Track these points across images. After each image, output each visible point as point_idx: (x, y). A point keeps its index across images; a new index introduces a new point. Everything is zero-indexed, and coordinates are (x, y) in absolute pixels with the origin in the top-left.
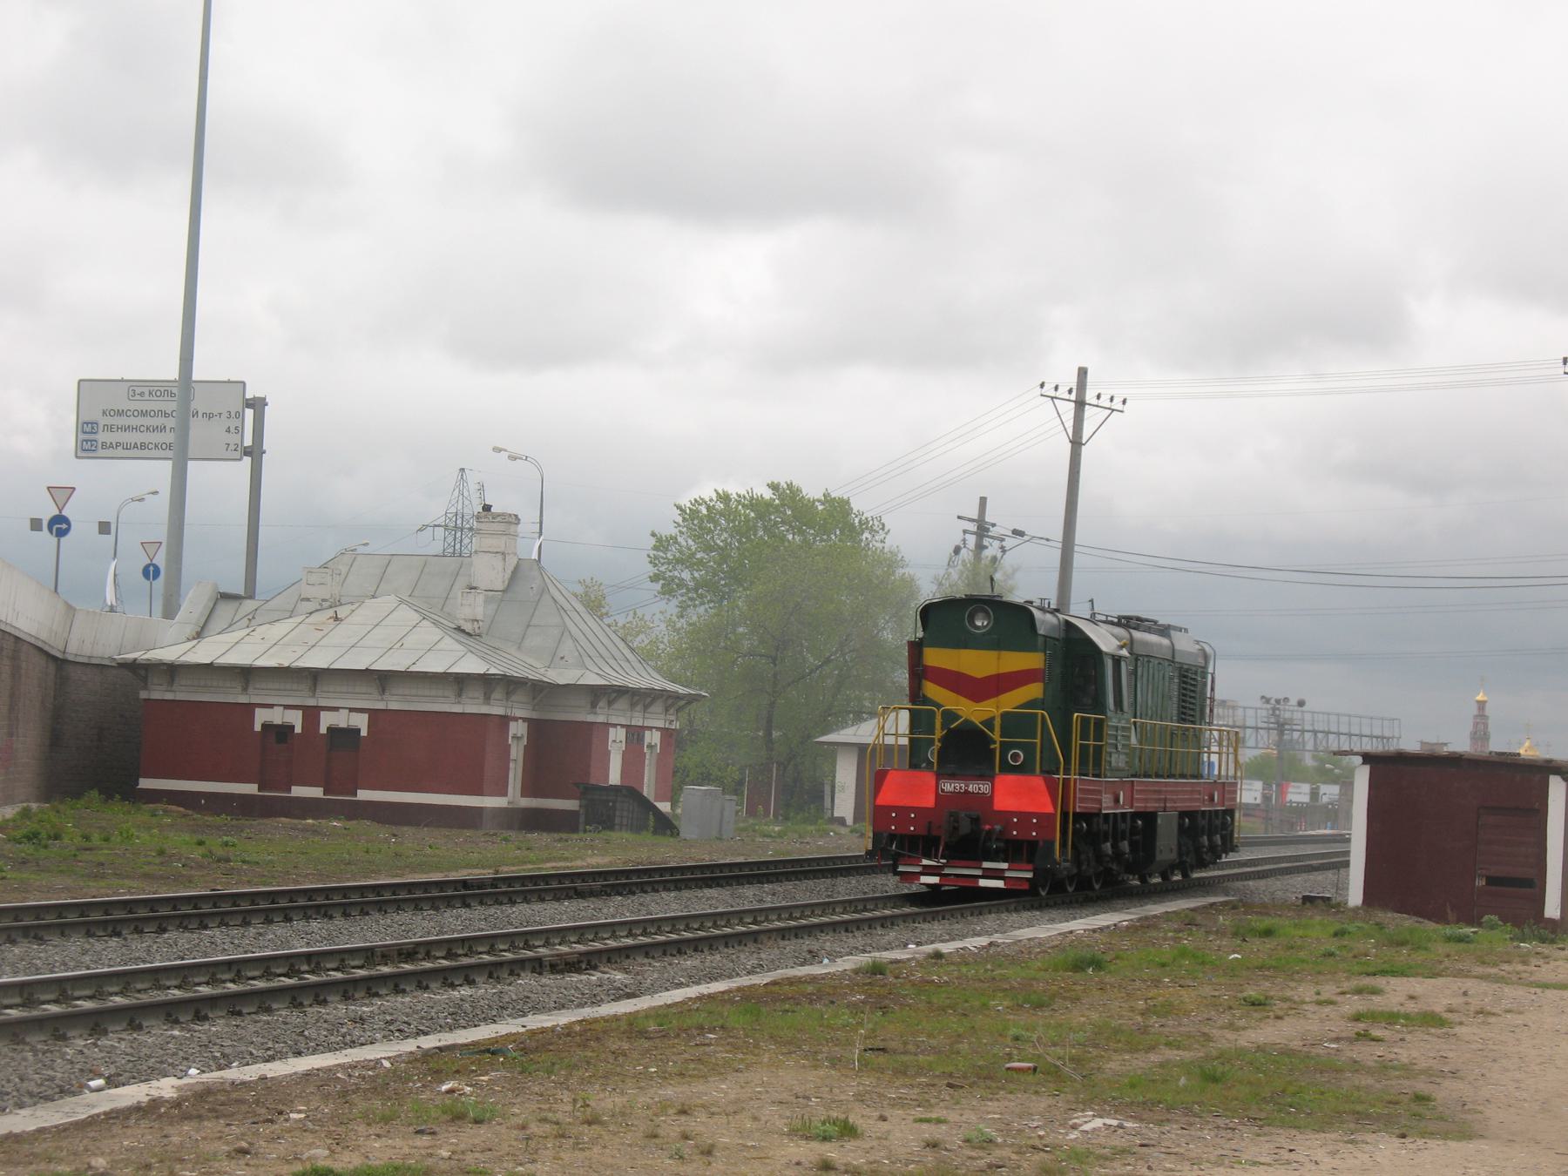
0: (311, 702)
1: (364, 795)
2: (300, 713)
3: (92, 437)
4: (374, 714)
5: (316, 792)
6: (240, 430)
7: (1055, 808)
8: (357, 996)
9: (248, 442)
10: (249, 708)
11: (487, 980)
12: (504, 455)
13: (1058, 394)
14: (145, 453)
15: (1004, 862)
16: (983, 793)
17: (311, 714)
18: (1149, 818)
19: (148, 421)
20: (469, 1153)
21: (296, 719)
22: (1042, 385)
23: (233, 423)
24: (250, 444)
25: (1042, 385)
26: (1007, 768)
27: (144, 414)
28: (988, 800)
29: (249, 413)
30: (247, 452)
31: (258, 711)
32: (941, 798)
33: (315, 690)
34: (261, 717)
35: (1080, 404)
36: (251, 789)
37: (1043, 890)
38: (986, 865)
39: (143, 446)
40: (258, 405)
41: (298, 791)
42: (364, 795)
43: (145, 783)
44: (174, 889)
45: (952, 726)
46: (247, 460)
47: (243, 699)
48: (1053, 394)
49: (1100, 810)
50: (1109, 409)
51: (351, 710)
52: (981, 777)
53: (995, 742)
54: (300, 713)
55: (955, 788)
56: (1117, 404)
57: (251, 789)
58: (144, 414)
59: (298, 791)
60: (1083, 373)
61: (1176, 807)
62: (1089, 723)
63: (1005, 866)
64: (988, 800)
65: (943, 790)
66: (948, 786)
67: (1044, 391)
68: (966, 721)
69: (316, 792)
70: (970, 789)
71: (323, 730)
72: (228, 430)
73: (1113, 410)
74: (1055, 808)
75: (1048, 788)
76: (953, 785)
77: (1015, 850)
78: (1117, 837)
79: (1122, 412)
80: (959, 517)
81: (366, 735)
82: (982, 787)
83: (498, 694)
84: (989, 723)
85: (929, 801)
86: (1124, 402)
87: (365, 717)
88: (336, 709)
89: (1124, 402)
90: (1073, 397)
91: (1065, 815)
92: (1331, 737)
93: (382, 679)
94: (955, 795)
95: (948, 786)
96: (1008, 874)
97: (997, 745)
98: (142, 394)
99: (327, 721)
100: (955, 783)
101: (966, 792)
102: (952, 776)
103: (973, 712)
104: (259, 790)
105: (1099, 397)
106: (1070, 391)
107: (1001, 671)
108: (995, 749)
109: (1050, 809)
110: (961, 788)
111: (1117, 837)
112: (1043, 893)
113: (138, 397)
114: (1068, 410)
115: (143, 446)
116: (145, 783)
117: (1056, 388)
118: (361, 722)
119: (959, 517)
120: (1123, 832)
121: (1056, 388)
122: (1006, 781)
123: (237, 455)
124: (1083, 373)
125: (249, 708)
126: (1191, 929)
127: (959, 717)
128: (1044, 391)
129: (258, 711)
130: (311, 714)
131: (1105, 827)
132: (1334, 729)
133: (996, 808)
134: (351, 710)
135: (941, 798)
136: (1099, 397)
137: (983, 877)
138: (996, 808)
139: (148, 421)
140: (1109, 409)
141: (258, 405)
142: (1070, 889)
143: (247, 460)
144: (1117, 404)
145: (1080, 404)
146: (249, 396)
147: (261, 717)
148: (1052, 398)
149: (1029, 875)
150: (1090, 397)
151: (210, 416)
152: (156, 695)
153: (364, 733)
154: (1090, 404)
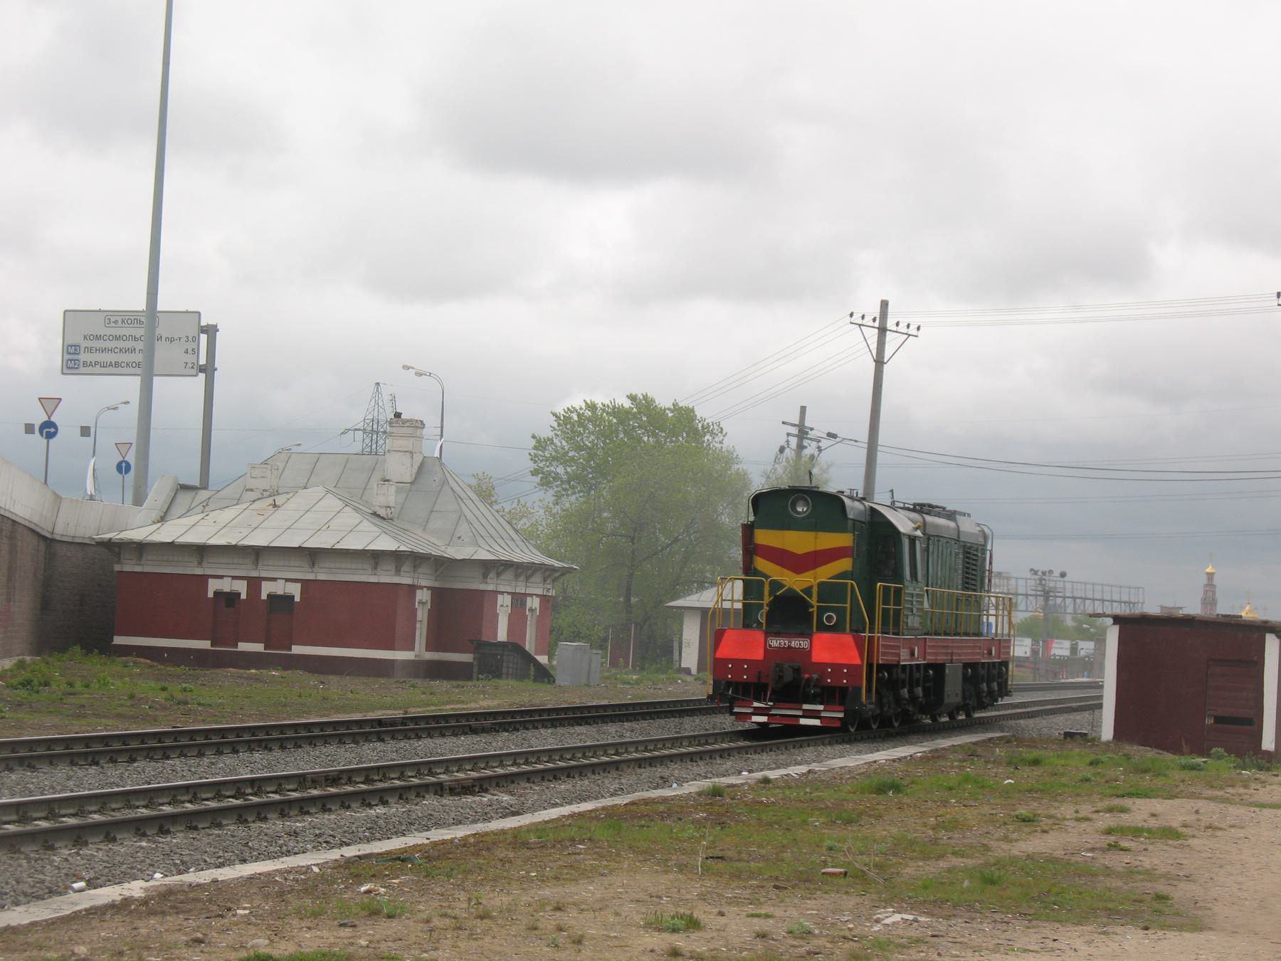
0: (254, 574)
1: (297, 650)
2: (245, 583)
3: (75, 357)
5: (258, 647)
6: (196, 352)
7: (862, 660)
9: (203, 361)
10: (204, 579)
13: (864, 322)
14: (119, 370)
16: (803, 648)
17: (254, 584)
19: (121, 344)
21: (241, 588)
22: (851, 315)
23: (191, 346)
24: (205, 363)
25: (851, 315)
27: (117, 338)
28: (807, 654)
29: (204, 337)
30: (202, 369)
31: (211, 581)
32: (768, 652)
33: (257, 564)
34: (213, 586)
35: (883, 330)
36: (205, 644)
39: (117, 365)
40: (211, 331)
41: (244, 647)
42: (297, 650)
43: (119, 640)
45: (778, 594)
46: (202, 376)
47: (198, 571)
48: (860, 322)
49: (899, 662)
50: (906, 334)
51: (287, 580)
52: (802, 635)
54: (245, 583)
55: (780, 644)
56: (912, 330)
57: (205, 644)
58: (117, 338)
59: (244, 647)
60: (884, 304)
61: (960, 660)
62: (890, 591)
64: (807, 654)
65: (770, 646)
66: (775, 643)
67: (853, 320)
68: (790, 589)
69: (258, 647)
70: (793, 645)
71: (264, 597)
72: (186, 352)
73: (909, 335)
74: (862, 660)
75: (856, 644)
76: (778, 642)
78: (912, 684)
79: (916, 336)
80: (783, 423)
82: (802, 643)
85: (759, 655)
86: (918, 328)
87: (299, 586)
88: (274, 579)
89: (918, 328)
90: (877, 324)
91: (870, 666)
93: (312, 555)
94: (780, 650)
95: (775, 643)
98: (116, 322)
99: (267, 589)
100: (780, 640)
101: (790, 647)
102: (778, 634)
103: (795, 581)
105: (897, 324)
106: (874, 320)
109: (858, 661)
110: (785, 644)
111: (912, 684)
113: (112, 325)
114: (873, 335)
115: (117, 365)
116: (119, 640)
117: (863, 317)
118: (295, 590)
119: (783, 423)
121: (863, 317)
122: (822, 638)
123: (194, 371)
124: (884, 304)
125: (204, 579)
127: (783, 586)
128: (853, 320)
129: (211, 581)
130: (254, 584)
131: (903, 676)
133: (813, 660)
134: (287, 580)
135: (768, 652)
136: (897, 324)
138: (813, 660)
139: (121, 344)
140: (906, 334)
141: (211, 331)
142: (874, 727)
143: (202, 376)
144: (912, 330)
145: (883, 330)
147: (213, 586)
148: (860, 325)
150: (890, 324)
151: (172, 340)
152: (127, 568)
153: (297, 599)
154: (890, 331)
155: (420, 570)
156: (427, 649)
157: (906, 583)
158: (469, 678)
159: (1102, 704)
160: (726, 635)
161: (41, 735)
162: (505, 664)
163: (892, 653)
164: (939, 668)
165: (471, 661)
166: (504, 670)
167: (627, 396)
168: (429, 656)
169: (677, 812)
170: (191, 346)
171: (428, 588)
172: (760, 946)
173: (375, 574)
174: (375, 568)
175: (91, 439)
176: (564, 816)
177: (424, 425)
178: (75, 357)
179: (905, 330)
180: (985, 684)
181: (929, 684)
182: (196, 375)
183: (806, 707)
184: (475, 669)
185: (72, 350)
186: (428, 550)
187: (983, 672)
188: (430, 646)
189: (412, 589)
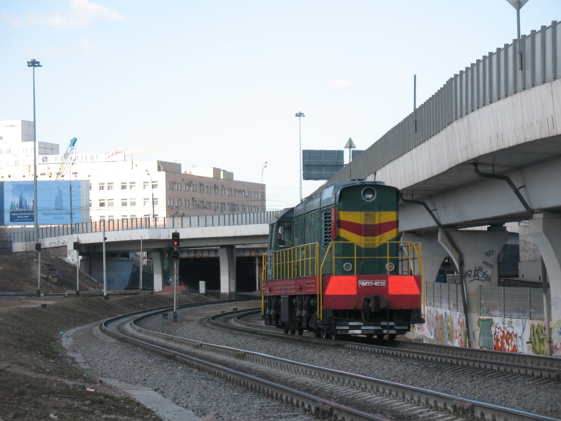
8: (244, 368)
11: (463, 405)
12: (147, 173)
16: (382, 286)
18: (279, 297)
20: (69, 336)
52: (380, 279)
55: (367, 284)
61: (287, 293)
65: (361, 285)
66: (364, 283)
76: (366, 282)
80: (415, 76)
81: (200, 282)
95: (364, 283)
100: (367, 281)
101: (374, 286)
110: (370, 284)
119: (415, 76)
126: (495, 349)
127: (385, 244)
135: (360, 289)
159: (161, 171)
163: (292, 284)
167: (350, 138)
169: (210, 407)
172: (399, 345)
175: (425, 281)
176: (112, 418)
183: (351, 324)
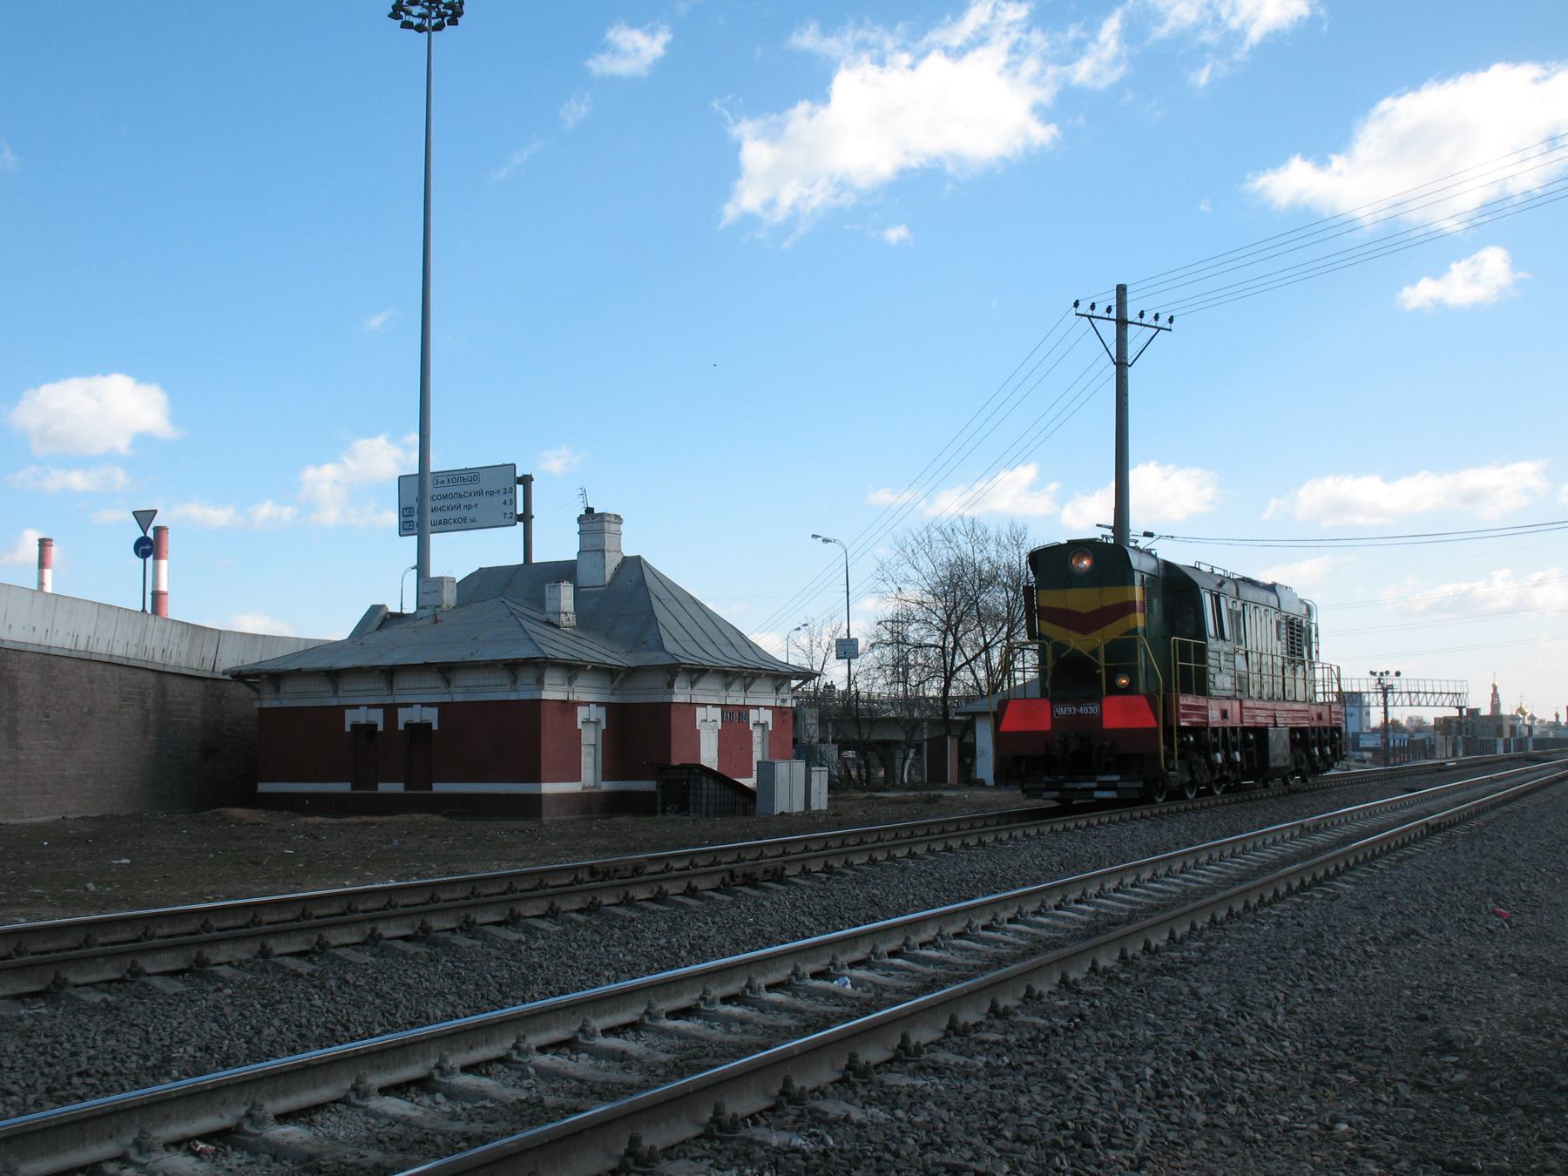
0: (389, 700)
1: (439, 788)
2: (381, 711)
3: (409, 519)
4: (442, 706)
5: (397, 788)
6: (513, 502)
7: (1157, 722)
9: (520, 511)
10: (340, 710)
13: (1095, 313)
14: (448, 527)
15: (1116, 774)
17: (391, 711)
19: (448, 502)
21: (377, 717)
22: (1076, 304)
23: (508, 497)
24: (522, 512)
25: (1076, 304)
26: (1114, 690)
27: (445, 497)
28: (1098, 719)
29: (520, 488)
30: (520, 518)
31: (400, 711)
32: (1055, 721)
33: (392, 686)
34: (351, 717)
35: (1122, 323)
36: (345, 787)
37: (1218, 790)
38: (1100, 778)
39: (446, 522)
40: (526, 481)
41: (385, 787)
42: (439, 788)
43: (264, 787)
44: (70, 914)
45: (1062, 656)
46: (520, 525)
47: (334, 702)
48: (1090, 313)
49: (1208, 723)
50: (1155, 327)
51: (423, 705)
53: (1100, 668)
54: (381, 711)
56: (1163, 322)
57: (345, 787)
58: (445, 497)
59: (385, 787)
60: (1121, 290)
62: (1189, 647)
63: (1117, 778)
64: (1098, 719)
65: (1057, 714)
67: (1079, 310)
68: (1074, 650)
69: (397, 788)
70: (1081, 711)
71: (401, 727)
72: (505, 503)
73: (1159, 329)
74: (1157, 722)
75: (1150, 705)
77: (1123, 763)
78: (1228, 748)
79: (1170, 330)
82: (1093, 709)
83: (736, 687)
84: (1095, 652)
85: (1046, 725)
86: (1171, 320)
87: (435, 711)
88: (410, 705)
89: (1171, 320)
90: (1113, 315)
91: (1168, 730)
92: (1421, 695)
93: (446, 670)
94: (1068, 717)
96: (1119, 785)
97: (1103, 670)
98: (442, 482)
99: (404, 716)
102: (1064, 701)
103: (1078, 642)
104: (406, 789)
105: (1142, 315)
106: (1109, 310)
107: (1105, 604)
108: (1100, 674)
109: (1154, 724)
111: (1228, 748)
112: (1218, 793)
113: (440, 485)
114: (1109, 330)
115: (446, 522)
116: (264, 787)
117: (1093, 307)
118: (432, 716)
120: (1326, 741)
121: (1093, 307)
122: (1112, 703)
123: (513, 521)
124: (1121, 290)
125: (340, 710)
127: (1068, 648)
128: (1079, 310)
129: (400, 711)
130: (391, 711)
131: (1214, 740)
132: (1422, 690)
133: (1105, 727)
134: (423, 705)
136: (1142, 315)
137: (1098, 789)
138: (1105, 727)
139: (448, 502)
140: (1155, 327)
141: (526, 481)
142: (1191, 796)
143: (520, 525)
144: (1163, 322)
145: (1122, 323)
146: (519, 474)
147: (351, 717)
148: (1089, 317)
149: (1140, 785)
150: (1132, 315)
151: (491, 493)
152: (266, 704)
153: (435, 727)
154: (1132, 323)
155: (577, 682)
156: (604, 779)
157: (1209, 640)
158: (652, 813)
160: (1010, 704)
161: (201, 898)
162: (692, 791)
164: (1261, 732)
165: (654, 789)
166: (691, 806)
168: (606, 786)
170: (508, 497)
171: (599, 704)
173: (515, 690)
174: (514, 682)
177: (621, 519)
178: (409, 519)
179: (1153, 323)
180: (1316, 749)
181: (1251, 749)
182: (515, 524)
184: (659, 799)
185: (406, 513)
186: (575, 653)
187: (1313, 737)
188: (609, 772)
189: (569, 707)
